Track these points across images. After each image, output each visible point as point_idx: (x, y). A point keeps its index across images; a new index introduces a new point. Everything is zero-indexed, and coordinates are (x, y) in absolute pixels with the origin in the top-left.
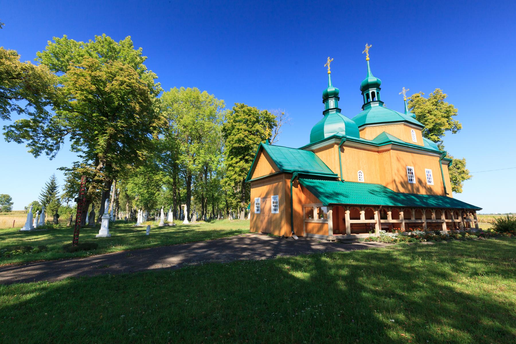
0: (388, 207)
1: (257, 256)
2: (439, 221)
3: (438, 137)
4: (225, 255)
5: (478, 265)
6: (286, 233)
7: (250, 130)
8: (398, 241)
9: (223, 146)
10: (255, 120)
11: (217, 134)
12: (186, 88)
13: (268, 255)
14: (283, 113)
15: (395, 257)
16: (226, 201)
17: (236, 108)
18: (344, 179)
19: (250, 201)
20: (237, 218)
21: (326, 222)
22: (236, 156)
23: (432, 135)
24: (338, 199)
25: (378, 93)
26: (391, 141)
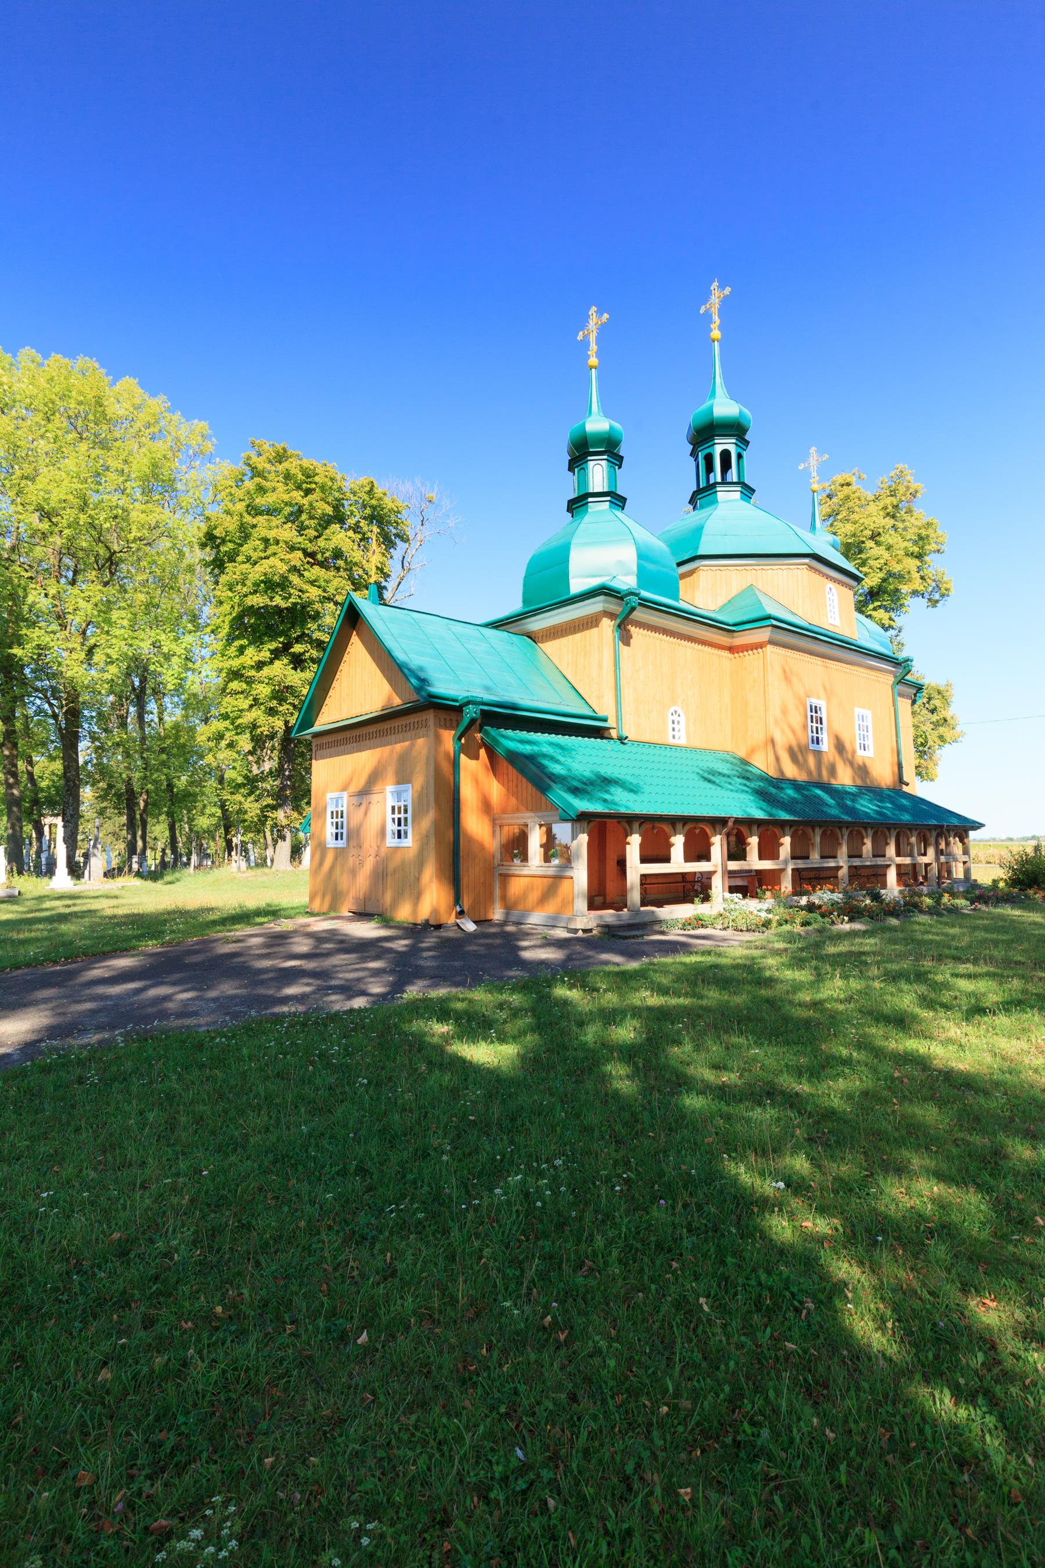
0: (750, 823)
1: (333, 998)
2: (880, 861)
3: (892, 614)
4: (215, 1000)
5: (981, 986)
6: (435, 912)
7: (310, 548)
8: (774, 924)
9: (206, 600)
10: (329, 510)
11: (181, 554)
12: (46, 356)
13: (377, 989)
14: (433, 495)
15: (768, 974)
16: (222, 806)
17: (255, 459)
18: (625, 734)
19: (309, 803)
20: (262, 863)
21: (568, 874)
22: (257, 641)
23: (875, 609)
24: (607, 796)
25: (740, 456)
26: (769, 617)
